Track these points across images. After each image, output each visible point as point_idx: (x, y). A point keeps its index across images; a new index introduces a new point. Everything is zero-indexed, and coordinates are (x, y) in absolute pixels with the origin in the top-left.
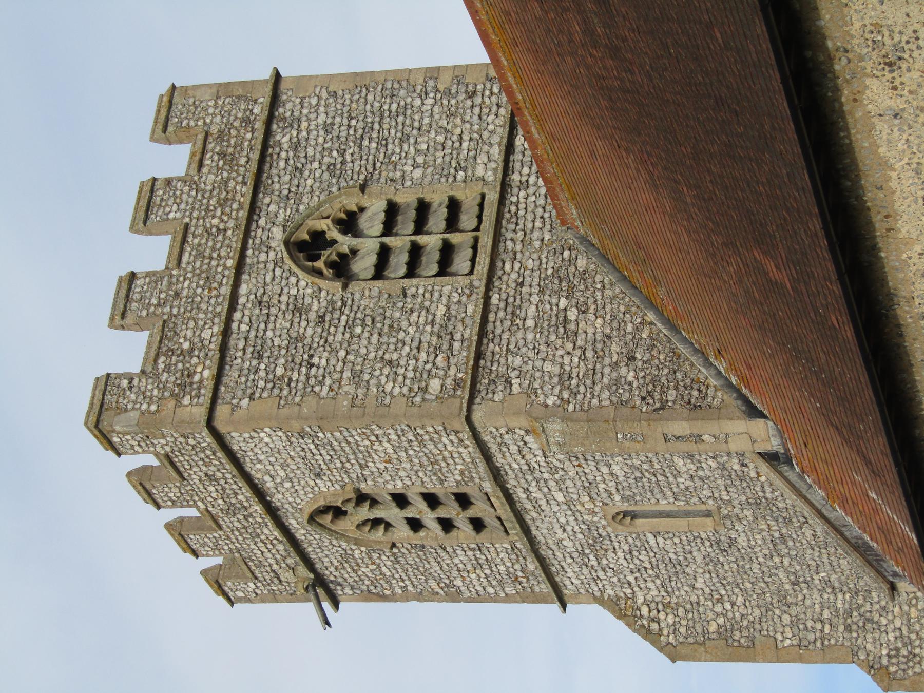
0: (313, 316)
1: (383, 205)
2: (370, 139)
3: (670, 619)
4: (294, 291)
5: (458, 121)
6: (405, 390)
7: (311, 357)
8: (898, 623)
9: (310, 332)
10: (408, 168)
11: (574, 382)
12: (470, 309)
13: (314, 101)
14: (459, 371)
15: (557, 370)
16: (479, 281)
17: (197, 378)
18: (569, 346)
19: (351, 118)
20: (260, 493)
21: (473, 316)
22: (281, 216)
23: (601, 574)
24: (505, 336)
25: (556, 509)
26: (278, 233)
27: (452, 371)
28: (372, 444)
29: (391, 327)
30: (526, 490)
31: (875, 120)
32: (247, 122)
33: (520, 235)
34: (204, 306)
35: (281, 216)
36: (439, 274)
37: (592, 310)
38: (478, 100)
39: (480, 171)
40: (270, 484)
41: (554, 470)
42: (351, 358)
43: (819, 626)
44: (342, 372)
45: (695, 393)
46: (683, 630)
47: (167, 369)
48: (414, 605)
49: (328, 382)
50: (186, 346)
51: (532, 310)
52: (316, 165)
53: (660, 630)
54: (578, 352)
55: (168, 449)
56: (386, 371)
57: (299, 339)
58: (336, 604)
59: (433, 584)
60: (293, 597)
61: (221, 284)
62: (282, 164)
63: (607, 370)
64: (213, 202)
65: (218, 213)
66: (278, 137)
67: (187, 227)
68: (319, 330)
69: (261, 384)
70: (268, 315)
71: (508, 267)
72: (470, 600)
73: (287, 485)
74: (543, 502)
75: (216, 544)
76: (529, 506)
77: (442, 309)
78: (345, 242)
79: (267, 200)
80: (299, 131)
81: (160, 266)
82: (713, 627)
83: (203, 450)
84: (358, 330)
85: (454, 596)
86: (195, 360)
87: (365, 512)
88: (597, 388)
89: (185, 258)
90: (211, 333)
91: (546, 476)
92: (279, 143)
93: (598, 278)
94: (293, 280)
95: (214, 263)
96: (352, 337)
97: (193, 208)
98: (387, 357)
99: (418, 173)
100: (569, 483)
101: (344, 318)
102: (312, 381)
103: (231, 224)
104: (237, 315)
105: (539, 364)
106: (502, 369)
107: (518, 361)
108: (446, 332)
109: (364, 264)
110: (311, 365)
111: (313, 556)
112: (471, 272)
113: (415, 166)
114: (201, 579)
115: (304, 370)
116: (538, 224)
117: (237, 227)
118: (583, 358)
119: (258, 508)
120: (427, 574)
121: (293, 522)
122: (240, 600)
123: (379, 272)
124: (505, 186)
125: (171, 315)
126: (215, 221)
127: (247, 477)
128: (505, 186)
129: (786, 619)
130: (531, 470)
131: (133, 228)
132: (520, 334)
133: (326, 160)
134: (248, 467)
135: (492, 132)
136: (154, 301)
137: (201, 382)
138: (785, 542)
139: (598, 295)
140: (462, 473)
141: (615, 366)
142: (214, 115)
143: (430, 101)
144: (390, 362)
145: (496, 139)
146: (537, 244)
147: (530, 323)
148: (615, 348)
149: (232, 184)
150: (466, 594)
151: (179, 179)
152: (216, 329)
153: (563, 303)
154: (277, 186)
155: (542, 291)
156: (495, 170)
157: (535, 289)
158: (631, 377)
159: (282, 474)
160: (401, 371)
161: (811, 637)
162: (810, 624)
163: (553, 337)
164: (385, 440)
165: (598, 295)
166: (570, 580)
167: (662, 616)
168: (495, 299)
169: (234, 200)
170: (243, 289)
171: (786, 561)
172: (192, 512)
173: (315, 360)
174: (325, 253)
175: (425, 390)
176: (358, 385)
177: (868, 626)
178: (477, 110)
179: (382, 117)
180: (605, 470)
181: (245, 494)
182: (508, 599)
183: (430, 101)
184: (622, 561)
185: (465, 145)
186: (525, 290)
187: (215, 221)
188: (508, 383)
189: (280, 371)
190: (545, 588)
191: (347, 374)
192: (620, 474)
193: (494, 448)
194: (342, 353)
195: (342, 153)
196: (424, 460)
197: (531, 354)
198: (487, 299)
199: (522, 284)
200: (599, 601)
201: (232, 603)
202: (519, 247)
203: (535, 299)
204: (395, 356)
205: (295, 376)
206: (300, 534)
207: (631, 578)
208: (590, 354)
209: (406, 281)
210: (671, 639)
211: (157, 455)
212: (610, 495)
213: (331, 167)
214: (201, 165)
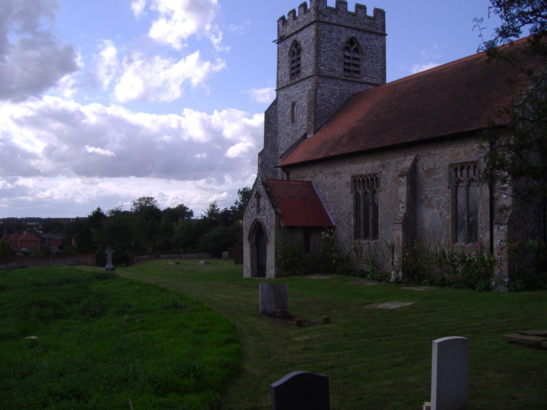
0: (337, 43)
1: (359, 57)
2: (372, 55)
3: (273, 112)
4: (342, 39)
5: (375, 73)
6: (322, 62)
7: (329, 42)
8: (271, 157)
9: (334, 42)
10: (366, 63)
11: (322, 96)
12: (337, 75)
13: (381, 43)
14: (325, 73)
15: (324, 93)
16: (343, 77)
17: (325, 18)
18: (329, 96)
19: (377, 51)
20: (301, 30)
21: (336, 76)
22: (358, 36)
23: (282, 99)
24: (332, 83)
25: (296, 91)
26: (354, 35)
27: (325, 72)
28: (311, 54)
29: (334, 59)
30: (300, 85)
31: (112, 104)
32: (377, 29)
33: (352, 86)
34: (340, 19)
35: (358, 36)
36: (344, 62)
37: (336, 100)
38: (379, 77)
39: (365, 78)
40: (303, 32)
41: (304, 91)
42: (328, 51)
43: (271, 141)
44: (326, 49)
45: (319, 121)
46: (271, 114)
47: (328, 12)
48: (277, 59)
49: (324, 46)
50: (332, 16)
51: (337, 88)
52: (368, 43)
53: (271, 110)
54: (328, 97)
55: (311, 11)
56: (326, 58)
57: (333, 40)
58: (276, 43)
59: (281, 64)
60: (278, 34)
61: (344, 23)
62: (368, 36)
63: (324, 103)
64: (361, 21)
65: (359, 23)
66: (374, 35)
67: (356, 16)
68: (334, 44)
69: (324, 32)
70: (338, 33)
71: (346, 83)
72: (277, 72)
73: (303, 36)
74: (298, 88)
75: (290, 19)
76: (297, 85)
77: (337, 69)
78: (352, 49)
79: (361, 33)
80: (375, 40)
81: (348, 10)
82: (271, 120)
83: (310, 19)
84: (334, 52)
85: (278, 68)
86: (329, 18)
87: (296, 51)
88: (321, 101)
89: (350, 15)
90: (334, 21)
91: (303, 89)
92: (372, 36)
93: (342, 102)
94: (344, 38)
95: (349, 22)
96: (333, 51)
97: (360, 17)
98: (328, 58)
99: (365, 65)
100: (302, 94)
101: (336, 49)
102: (324, 42)
103: (356, 25)
104: (338, 27)
105: (326, 89)
106: (325, 82)
107: (327, 85)
108: (333, 70)
109: (347, 54)
110: (327, 42)
111: (287, 40)
112: (345, 76)
113: (366, 64)
114: (283, 15)
115: (326, 41)
116: (354, 89)
117: (356, 26)
118: (327, 98)
119: (298, 29)
120: (283, 63)
121: (295, 36)
122: (278, 23)
123: (346, 57)
124: (361, 83)
125: (338, 12)
126: (357, 22)
127: (304, 28)
128: (361, 83)
129: (273, 135)
130: (304, 87)
131: (357, 4)
132: (332, 85)
133: (369, 46)
134: (307, 28)
135: (372, 80)
136: (341, 9)
137: (325, 19)
138: (288, 136)
139: (339, 102)
140: (304, 72)
141: (325, 105)
142: (379, 22)
143: (379, 67)
144: (327, 59)
145: (371, 81)
146: (349, 89)
147: (334, 88)
148: (329, 105)
149: (365, 25)
150: (279, 71)
151: (366, 14)
152: (335, 22)
153: (338, 94)
154: (364, 35)
155: (340, 90)
156: (365, 81)
157: (341, 89)
158: (323, 108)
159: (305, 35)
160: (326, 61)
161: (269, 140)
162: (271, 140)
163: (331, 92)
164: (312, 57)
165: (339, 102)
166: (282, 93)
167: (274, 110)
168: (339, 80)
169: (361, 26)
170: (343, 28)
171: (284, 136)
172: (297, 15)
173: (328, 43)
174: (350, 45)
175: (321, 66)
176: (323, 52)
177: (271, 151)
178: (377, 77)
179: (376, 57)
180: (304, 101)
181: (301, 26)
182: (277, 79)
183: (379, 67)
184: (285, 103)
185: (370, 75)
186: (341, 87)
187: (357, 22)
188: (322, 83)
189: (326, 36)
190: (280, 87)
191: (325, 50)
192: (303, 104)
193: (309, 79)
194: (329, 49)
195: (370, 49)
196: (307, 65)
197: (328, 88)
198: (339, 79)
199: (342, 86)
200: (277, 98)
201: (278, 21)
202: (349, 85)
203: (339, 89)
204: (328, 60)
205: (325, 39)
206: (292, 37)
207: (281, 105)
208: (328, 100)
209: (343, 62)
210: (269, 112)
211: (310, 9)
212: (299, 102)
213: (367, 46)
214: (369, 19)
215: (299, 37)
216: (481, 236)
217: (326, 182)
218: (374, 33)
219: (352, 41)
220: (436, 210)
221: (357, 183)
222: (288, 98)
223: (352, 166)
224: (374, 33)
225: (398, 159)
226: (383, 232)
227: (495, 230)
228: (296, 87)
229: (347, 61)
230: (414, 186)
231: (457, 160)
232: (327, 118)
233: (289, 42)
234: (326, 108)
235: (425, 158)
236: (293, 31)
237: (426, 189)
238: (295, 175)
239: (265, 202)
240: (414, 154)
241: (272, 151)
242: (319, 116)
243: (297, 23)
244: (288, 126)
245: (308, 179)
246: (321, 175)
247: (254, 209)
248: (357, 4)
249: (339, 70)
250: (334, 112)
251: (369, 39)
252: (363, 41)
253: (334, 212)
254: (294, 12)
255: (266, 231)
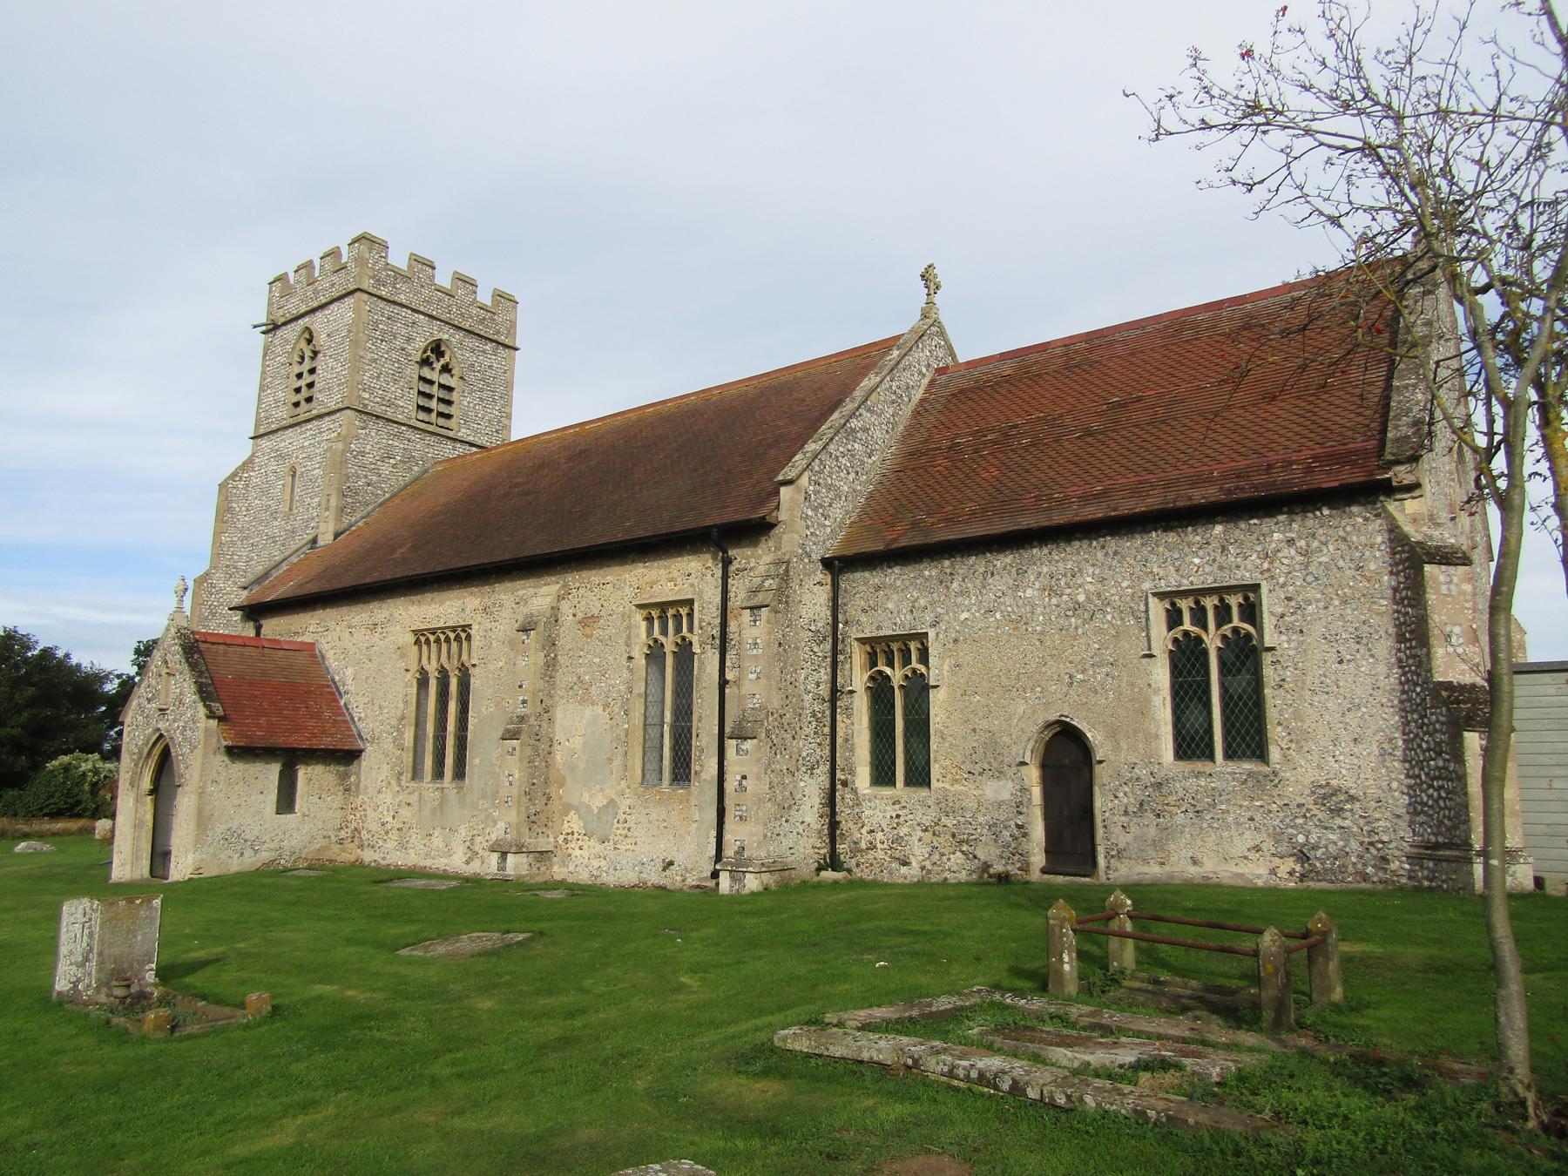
16: (413, 422)
20: (322, 307)
26: (446, 337)
39: (463, 430)
40: (327, 312)
47: (388, 275)
59: (270, 379)
72: (259, 395)
77: (402, 404)
87: (308, 354)
90: (402, 298)
99: (466, 403)
109: (426, 373)
118: (371, 463)
119: (316, 304)
120: (274, 378)
122: (271, 288)
123: (421, 379)
131: (455, 272)
141: (366, 477)
144: (379, 377)
145: (476, 439)
147: (391, 442)
155: (404, 449)
161: (225, 549)
166: (264, 443)
170: (422, 317)
182: (258, 413)
189: (381, 326)
190: (262, 431)
200: (253, 455)
206: (301, 322)
215: (318, 322)
216: (698, 768)
217: (350, 644)
218: (492, 341)
219: (437, 349)
220: (599, 710)
221: (425, 648)
222: (281, 457)
223: (414, 609)
224: (492, 341)
225: (521, 593)
226: (477, 761)
227: (731, 752)
228: (301, 434)
229: (426, 388)
230: (553, 655)
231: (651, 597)
232: (370, 507)
233: (291, 332)
234: (369, 485)
235: (582, 591)
236: (303, 309)
237: (581, 661)
238: (274, 627)
239: (184, 686)
240: (558, 583)
241: (231, 577)
242: (350, 500)
243: (316, 292)
244: (276, 519)
245: (307, 639)
246: (338, 628)
247: (154, 705)
248: (455, 272)
249: (406, 406)
250: (387, 495)
251: (479, 351)
252: (461, 351)
253: (363, 715)
254: (308, 266)
255: (178, 760)
